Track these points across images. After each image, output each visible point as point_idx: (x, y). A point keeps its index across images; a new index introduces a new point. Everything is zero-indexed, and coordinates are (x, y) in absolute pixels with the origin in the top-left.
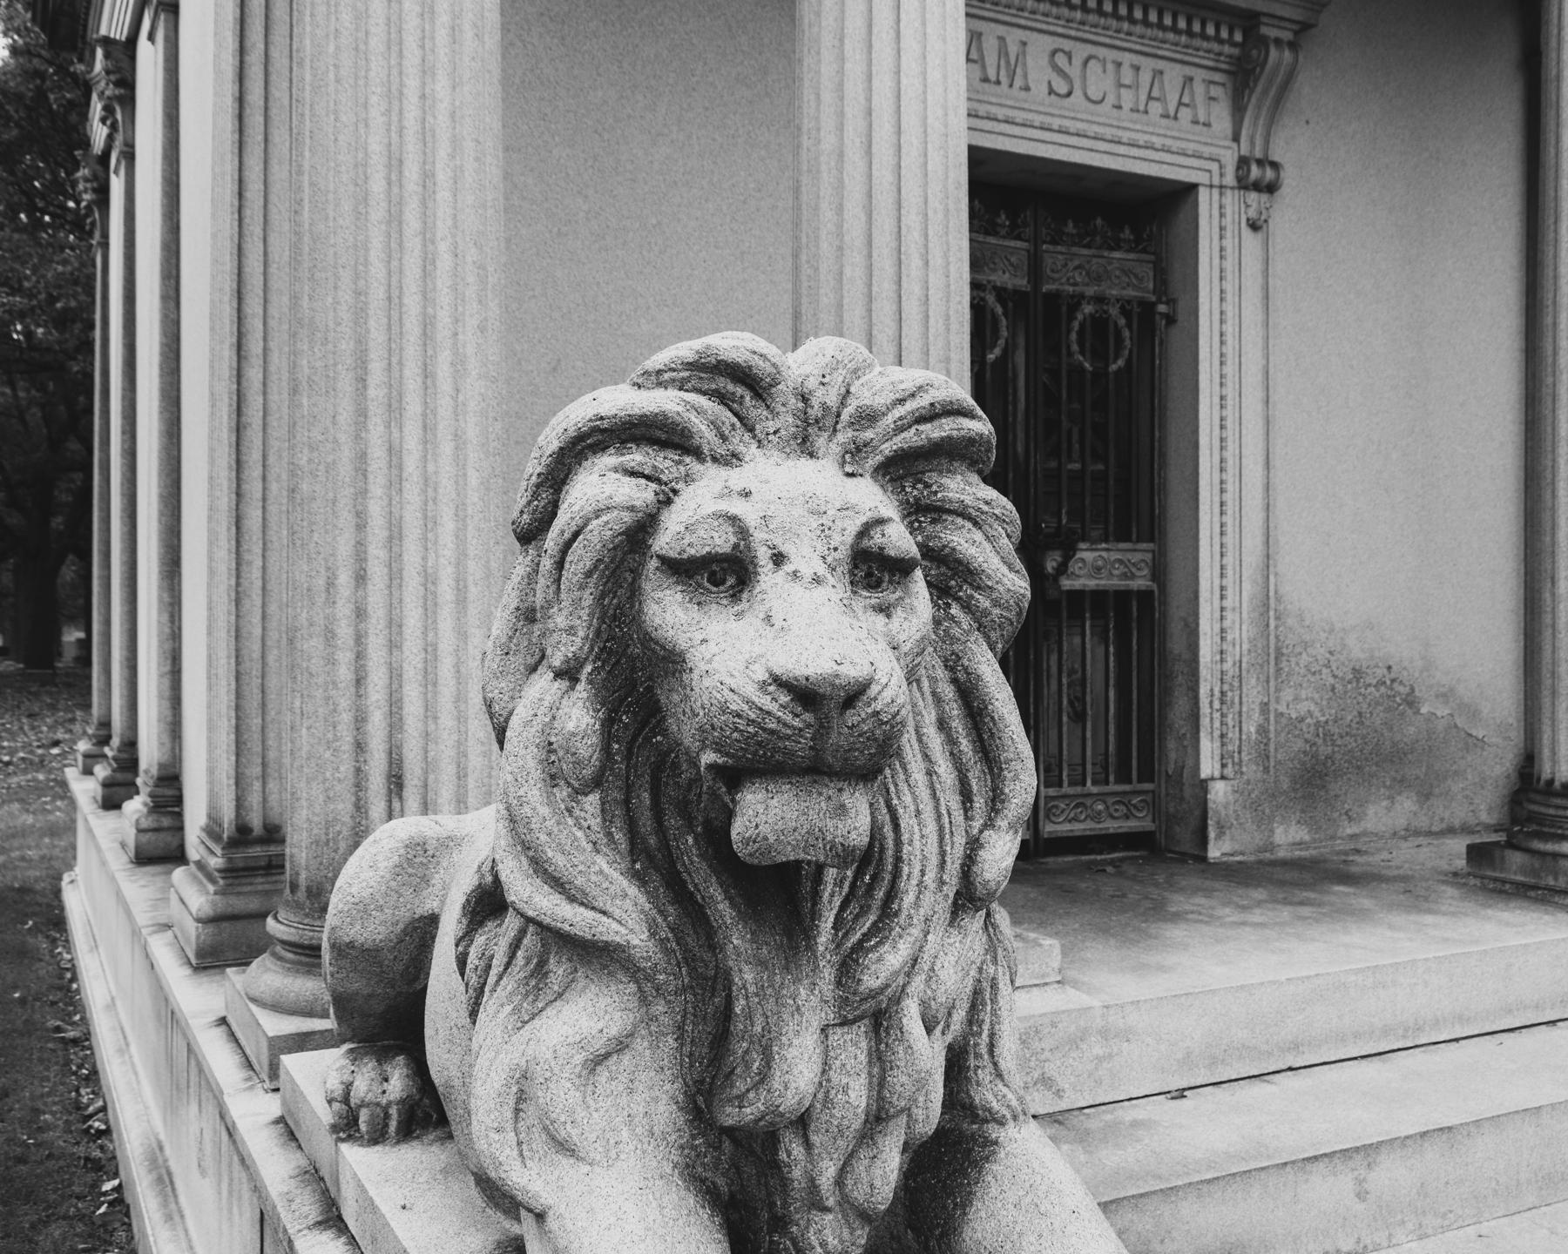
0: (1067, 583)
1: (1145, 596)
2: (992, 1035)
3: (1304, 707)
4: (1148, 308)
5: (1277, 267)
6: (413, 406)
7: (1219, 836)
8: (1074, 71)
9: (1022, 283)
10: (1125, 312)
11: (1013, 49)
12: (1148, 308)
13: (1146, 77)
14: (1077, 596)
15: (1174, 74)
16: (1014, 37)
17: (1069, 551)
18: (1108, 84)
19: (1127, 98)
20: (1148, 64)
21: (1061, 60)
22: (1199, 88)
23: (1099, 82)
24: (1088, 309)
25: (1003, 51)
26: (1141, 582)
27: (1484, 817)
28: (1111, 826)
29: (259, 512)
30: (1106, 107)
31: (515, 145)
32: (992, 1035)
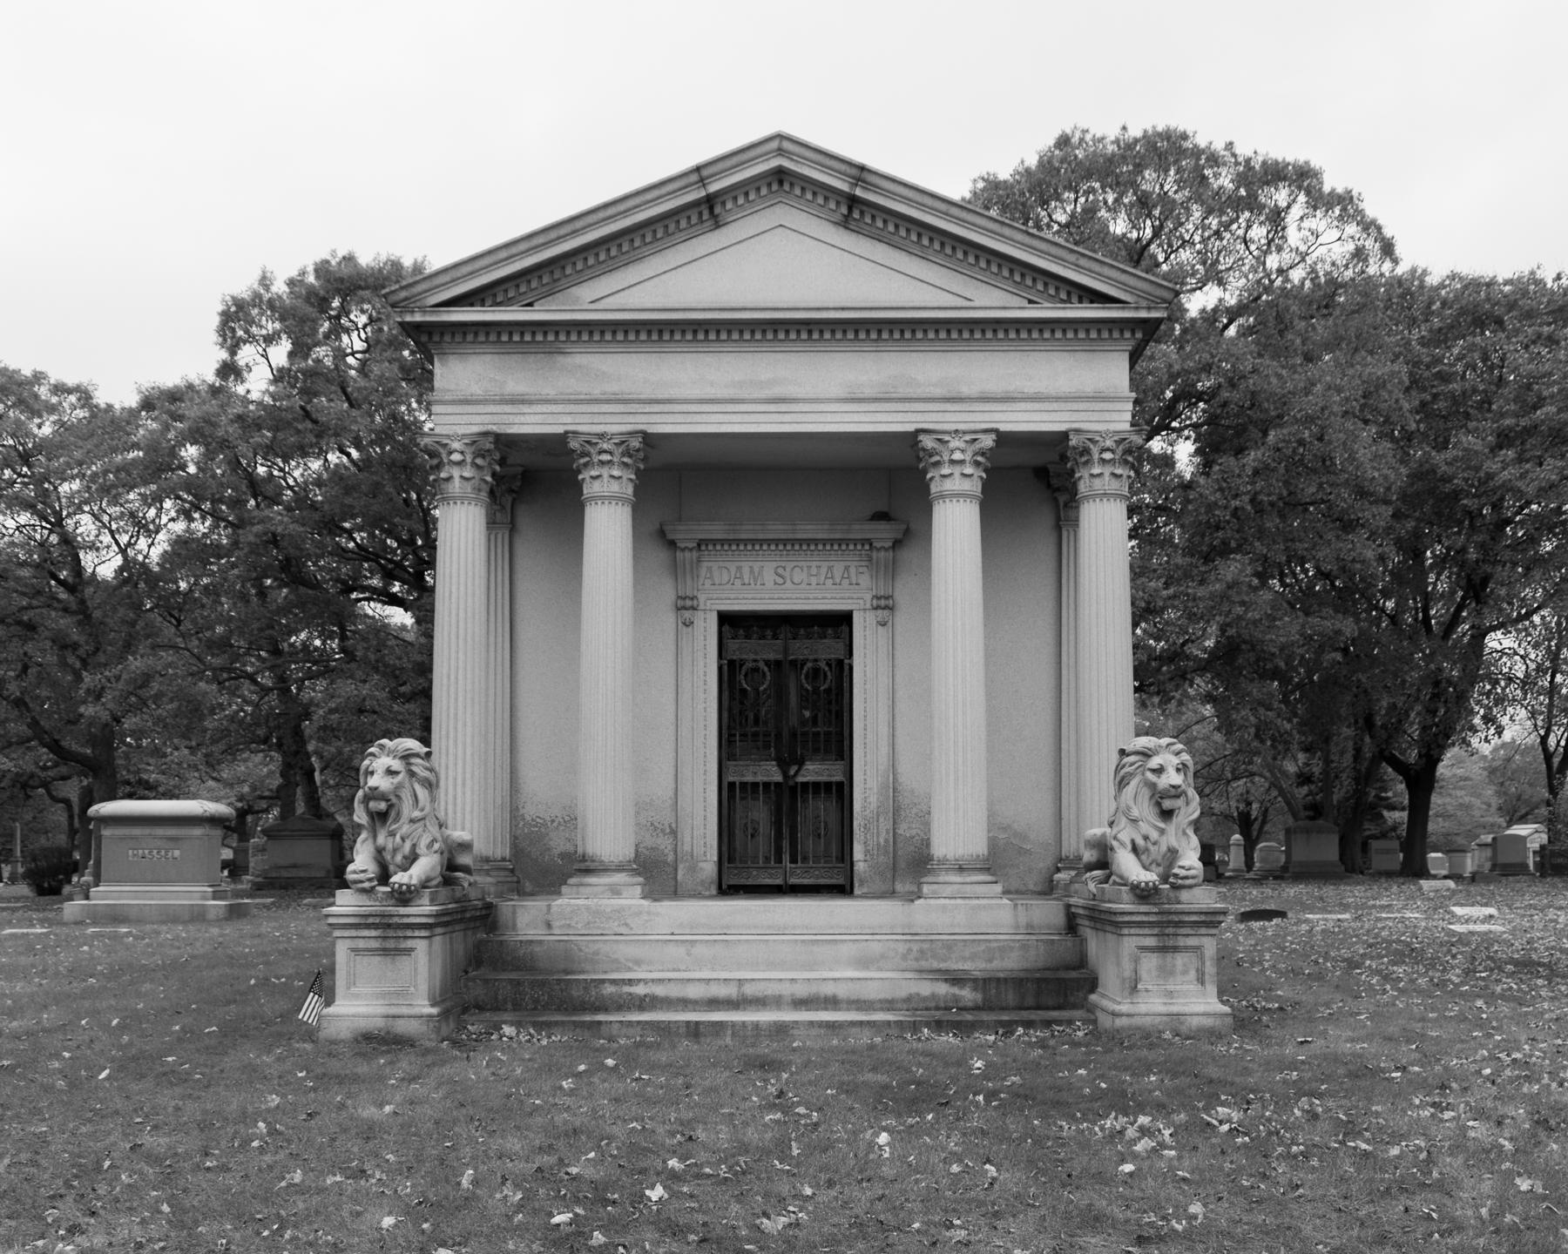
0: (800, 779)
1: (840, 785)
2: (800, 1003)
3: (914, 832)
4: (840, 663)
5: (898, 639)
6: (452, 735)
7: (861, 885)
8: (787, 574)
9: (780, 657)
10: (829, 665)
11: (756, 570)
12: (840, 663)
13: (824, 570)
14: (805, 785)
15: (838, 568)
16: (756, 566)
17: (801, 763)
18: (804, 575)
19: (814, 580)
20: (825, 565)
21: (780, 571)
22: (853, 570)
23: (799, 576)
24: (809, 665)
25: (752, 571)
26: (838, 778)
27: (1031, 887)
28: (822, 881)
29: (476, 390)
30: (803, 586)
31: (635, 549)
32: (800, 1003)
